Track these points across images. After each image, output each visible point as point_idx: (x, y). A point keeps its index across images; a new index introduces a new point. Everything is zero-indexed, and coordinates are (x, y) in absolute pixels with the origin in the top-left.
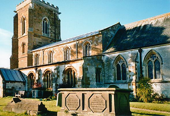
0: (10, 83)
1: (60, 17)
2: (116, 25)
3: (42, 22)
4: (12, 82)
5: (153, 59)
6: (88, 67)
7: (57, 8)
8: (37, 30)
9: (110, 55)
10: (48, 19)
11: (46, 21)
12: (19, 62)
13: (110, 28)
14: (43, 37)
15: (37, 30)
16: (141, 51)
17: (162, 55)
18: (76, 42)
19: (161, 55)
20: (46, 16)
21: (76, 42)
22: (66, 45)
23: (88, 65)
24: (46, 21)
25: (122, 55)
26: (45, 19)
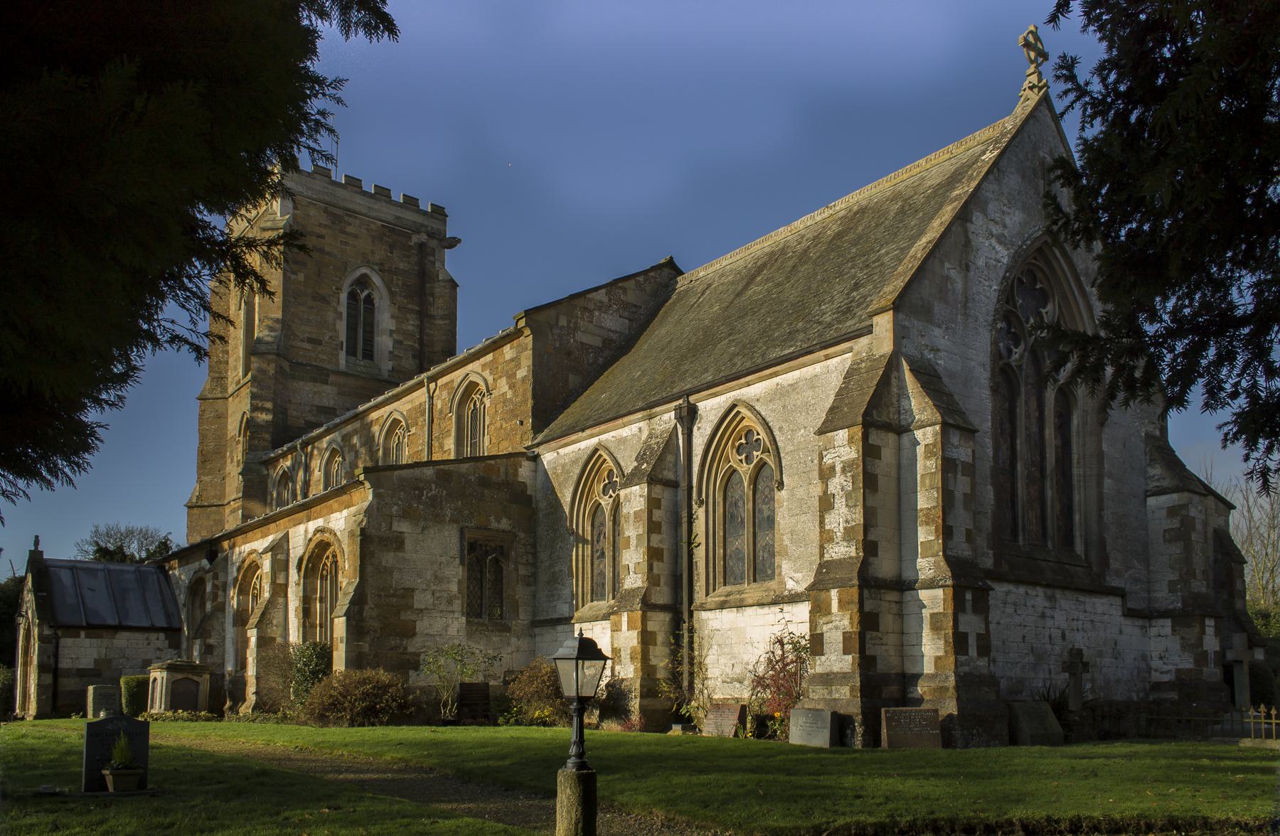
0: (87, 637)
1: (452, 263)
2: (645, 272)
3: (344, 297)
4: (96, 629)
5: (748, 459)
6: (404, 527)
7: (439, 212)
8: (310, 340)
9: (562, 451)
10: (376, 280)
11: (366, 293)
12: (1247, 570)
13: (601, 296)
14: (341, 380)
15: (310, 340)
16: (689, 416)
17: (781, 429)
18: (425, 389)
19: (776, 433)
20: (367, 263)
21: (425, 389)
22: (388, 409)
23: (406, 515)
24: (366, 293)
25: (610, 445)
26: (363, 282)
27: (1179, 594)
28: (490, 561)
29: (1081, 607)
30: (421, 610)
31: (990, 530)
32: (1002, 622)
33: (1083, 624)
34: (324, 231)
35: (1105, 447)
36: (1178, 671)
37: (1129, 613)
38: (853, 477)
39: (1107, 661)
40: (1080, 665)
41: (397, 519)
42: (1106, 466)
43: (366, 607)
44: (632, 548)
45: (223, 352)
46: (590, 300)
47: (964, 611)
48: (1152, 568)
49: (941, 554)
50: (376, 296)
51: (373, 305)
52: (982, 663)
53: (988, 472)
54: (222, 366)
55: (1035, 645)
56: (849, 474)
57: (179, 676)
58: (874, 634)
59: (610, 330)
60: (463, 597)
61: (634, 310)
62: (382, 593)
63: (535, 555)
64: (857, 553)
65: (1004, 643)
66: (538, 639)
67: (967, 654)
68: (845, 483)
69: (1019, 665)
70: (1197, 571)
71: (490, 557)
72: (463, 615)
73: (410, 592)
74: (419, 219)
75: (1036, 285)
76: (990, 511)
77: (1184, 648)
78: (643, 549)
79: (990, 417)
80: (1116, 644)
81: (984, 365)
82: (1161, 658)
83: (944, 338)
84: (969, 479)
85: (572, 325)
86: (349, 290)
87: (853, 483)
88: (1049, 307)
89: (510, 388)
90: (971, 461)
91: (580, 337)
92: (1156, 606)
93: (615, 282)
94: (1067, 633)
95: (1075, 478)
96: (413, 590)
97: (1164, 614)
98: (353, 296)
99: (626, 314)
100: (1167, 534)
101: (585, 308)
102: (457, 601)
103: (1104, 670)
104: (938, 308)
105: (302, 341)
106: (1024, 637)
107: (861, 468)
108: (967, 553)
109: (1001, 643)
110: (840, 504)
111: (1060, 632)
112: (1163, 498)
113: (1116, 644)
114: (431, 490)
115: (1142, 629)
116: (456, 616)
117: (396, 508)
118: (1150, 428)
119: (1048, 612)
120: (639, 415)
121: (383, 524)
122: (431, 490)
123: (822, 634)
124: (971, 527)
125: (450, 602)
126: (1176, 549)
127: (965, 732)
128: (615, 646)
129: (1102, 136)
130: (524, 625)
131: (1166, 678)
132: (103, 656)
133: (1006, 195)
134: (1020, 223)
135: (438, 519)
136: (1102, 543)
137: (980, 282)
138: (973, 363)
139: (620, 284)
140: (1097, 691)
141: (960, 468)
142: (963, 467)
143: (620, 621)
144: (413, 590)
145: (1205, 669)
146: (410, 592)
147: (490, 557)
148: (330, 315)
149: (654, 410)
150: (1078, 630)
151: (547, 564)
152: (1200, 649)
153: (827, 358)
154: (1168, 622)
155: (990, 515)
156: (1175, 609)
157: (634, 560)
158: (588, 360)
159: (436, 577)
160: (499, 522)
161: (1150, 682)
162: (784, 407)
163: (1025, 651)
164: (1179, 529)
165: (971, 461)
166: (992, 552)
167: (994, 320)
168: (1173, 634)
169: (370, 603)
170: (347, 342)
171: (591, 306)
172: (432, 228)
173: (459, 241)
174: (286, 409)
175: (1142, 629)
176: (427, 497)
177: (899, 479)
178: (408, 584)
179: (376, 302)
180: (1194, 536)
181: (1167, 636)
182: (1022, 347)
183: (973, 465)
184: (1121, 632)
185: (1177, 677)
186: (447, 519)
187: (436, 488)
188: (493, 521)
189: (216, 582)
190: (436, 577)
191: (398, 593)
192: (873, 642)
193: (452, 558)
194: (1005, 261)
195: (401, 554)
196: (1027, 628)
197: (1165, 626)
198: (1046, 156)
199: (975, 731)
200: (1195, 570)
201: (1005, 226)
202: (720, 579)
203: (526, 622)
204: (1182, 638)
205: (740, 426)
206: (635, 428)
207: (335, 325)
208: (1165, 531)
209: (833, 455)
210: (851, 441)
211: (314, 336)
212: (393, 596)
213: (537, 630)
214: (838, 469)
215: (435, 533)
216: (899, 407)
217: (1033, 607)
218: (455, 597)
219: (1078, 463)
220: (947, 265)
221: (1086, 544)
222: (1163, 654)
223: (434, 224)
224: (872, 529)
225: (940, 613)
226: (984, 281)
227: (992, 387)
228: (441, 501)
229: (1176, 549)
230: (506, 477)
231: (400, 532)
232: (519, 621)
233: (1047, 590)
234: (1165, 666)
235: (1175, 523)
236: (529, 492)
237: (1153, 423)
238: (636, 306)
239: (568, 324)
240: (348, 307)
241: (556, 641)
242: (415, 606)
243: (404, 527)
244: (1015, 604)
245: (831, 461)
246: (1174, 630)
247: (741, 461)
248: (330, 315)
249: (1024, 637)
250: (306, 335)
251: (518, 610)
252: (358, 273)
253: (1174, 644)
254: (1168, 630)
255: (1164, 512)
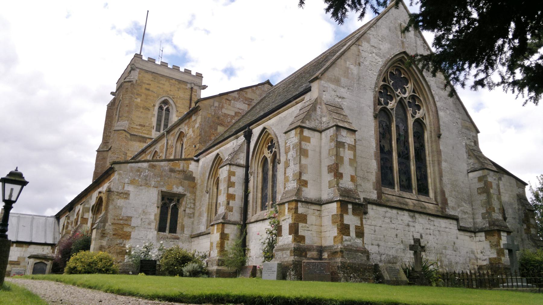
0: (16, 246)
3: (156, 108)
6: (130, 188)
8: (140, 125)
9: (207, 157)
11: (166, 106)
13: (235, 94)
15: (140, 125)
24: (166, 106)
27: (487, 219)
28: (172, 205)
29: (432, 223)
30: (134, 227)
31: (375, 181)
32: (455, 256)
33: (433, 231)
34: (150, 82)
35: (441, 148)
36: (490, 259)
37: (462, 229)
38: (296, 150)
39: (449, 252)
40: (419, 247)
41: (127, 184)
42: (443, 156)
43: (107, 224)
44: (222, 195)
45: (109, 132)
46: (230, 96)
47: (347, 213)
48: (474, 207)
49: (336, 186)
50: (170, 108)
51: (169, 112)
52: (359, 241)
53: (373, 154)
54: (108, 137)
55: (403, 240)
56: (295, 150)
57: (38, 261)
58: (304, 225)
59: (239, 109)
60: (156, 222)
61: (250, 100)
62: (116, 218)
63: (194, 204)
64: (297, 186)
65: (384, 236)
66: (193, 243)
67: (349, 235)
68: (293, 154)
69: (394, 249)
70: (496, 209)
71: (172, 204)
72: (155, 230)
73: (129, 218)
74: (191, 78)
75: (401, 75)
76: (374, 172)
77: (491, 246)
78: (225, 195)
79: (373, 129)
80: (454, 243)
81: (369, 106)
82: (482, 252)
83: (346, 93)
84: (352, 152)
85: (221, 106)
86: (160, 105)
87: (296, 153)
88: (409, 85)
89: (193, 132)
90: (353, 144)
91: (224, 111)
92: (477, 226)
93: (241, 90)
94: (423, 235)
95: (428, 162)
96: (131, 217)
97: (481, 231)
98: (161, 108)
99: (247, 102)
100: (479, 190)
101: (227, 99)
102: (153, 224)
103: (448, 257)
104: (343, 80)
105: (137, 125)
106: (397, 235)
107: (299, 146)
108: (352, 187)
109: (383, 236)
110: (291, 163)
111: (419, 234)
112: (476, 173)
113: (454, 243)
114: (145, 173)
115: (470, 237)
116: (152, 231)
117: (127, 180)
118: (468, 142)
119: (411, 224)
120: (233, 137)
121: (120, 187)
122: (145, 173)
123: (281, 226)
124: (353, 174)
125: (149, 224)
126: (484, 197)
127: (346, 275)
128: (212, 241)
129: (513, 52)
130: (186, 237)
131: (485, 263)
132: (22, 256)
133: (381, 37)
134: (388, 48)
135: (147, 185)
136: (443, 193)
137: (367, 71)
138: (363, 105)
139: (245, 90)
140: (444, 267)
141: (347, 146)
142: (349, 146)
143: (214, 229)
144: (131, 217)
145: (503, 258)
146: (129, 218)
147: (172, 204)
148: (149, 116)
149: (238, 134)
150: (430, 234)
151: (199, 208)
152: (499, 247)
153: (297, 103)
154: (483, 234)
155: (374, 173)
156: (486, 227)
157: (222, 200)
158: (227, 121)
159: (144, 212)
160: (178, 188)
161: (477, 265)
162: (282, 127)
163: (398, 242)
164: (484, 188)
165: (353, 144)
166: (376, 191)
167: (375, 87)
168: (486, 240)
169: (109, 222)
170: (156, 127)
171: (230, 99)
172: (196, 82)
173: (207, 86)
174: (126, 153)
175: (470, 237)
176: (143, 176)
177: (320, 153)
178: (129, 215)
179: (171, 110)
180: (492, 191)
181: (483, 241)
182: (394, 101)
183: (355, 146)
184: (457, 238)
185: (490, 262)
186: (152, 186)
187: (148, 172)
188: (175, 188)
189: (69, 221)
190: (144, 212)
191: (124, 218)
192: (303, 229)
193: (153, 203)
194: (381, 63)
195: (127, 201)
196: (399, 231)
197: (482, 236)
198: (402, 22)
199: (352, 275)
200: (494, 208)
201: (380, 49)
202: (259, 208)
203: (187, 235)
204: (490, 242)
205: (268, 138)
206: (231, 143)
207: (151, 119)
208: (478, 189)
209: (290, 142)
210: (296, 134)
211: (142, 124)
212: (121, 220)
213: (193, 239)
214: (291, 148)
215: (145, 192)
216: (321, 121)
217: (402, 220)
218: (152, 222)
219: (429, 155)
220: (348, 63)
221: (435, 193)
222: (482, 251)
223: (197, 80)
224: (304, 175)
225: (335, 214)
226: (369, 71)
227: (374, 116)
228: (150, 178)
229: (484, 197)
230: (183, 168)
231: (128, 191)
232: (184, 235)
233: (410, 213)
234: (484, 257)
235: (482, 185)
236: (194, 176)
237: (469, 139)
238: (251, 99)
239: (219, 105)
240: (158, 113)
241: (199, 244)
242: (132, 225)
243: (130, 188)
244: (391, 218)
245: (289, 145)
246: (486, 238)
247: (269, 153)
248: (149, 116)
249: (397, 235)
250: (138, 123)
251: (184, 230)
252: (163, 99)
253: (486, 244)
254: (483, 238)
255: (477, 180)
